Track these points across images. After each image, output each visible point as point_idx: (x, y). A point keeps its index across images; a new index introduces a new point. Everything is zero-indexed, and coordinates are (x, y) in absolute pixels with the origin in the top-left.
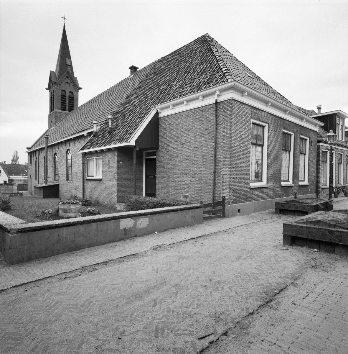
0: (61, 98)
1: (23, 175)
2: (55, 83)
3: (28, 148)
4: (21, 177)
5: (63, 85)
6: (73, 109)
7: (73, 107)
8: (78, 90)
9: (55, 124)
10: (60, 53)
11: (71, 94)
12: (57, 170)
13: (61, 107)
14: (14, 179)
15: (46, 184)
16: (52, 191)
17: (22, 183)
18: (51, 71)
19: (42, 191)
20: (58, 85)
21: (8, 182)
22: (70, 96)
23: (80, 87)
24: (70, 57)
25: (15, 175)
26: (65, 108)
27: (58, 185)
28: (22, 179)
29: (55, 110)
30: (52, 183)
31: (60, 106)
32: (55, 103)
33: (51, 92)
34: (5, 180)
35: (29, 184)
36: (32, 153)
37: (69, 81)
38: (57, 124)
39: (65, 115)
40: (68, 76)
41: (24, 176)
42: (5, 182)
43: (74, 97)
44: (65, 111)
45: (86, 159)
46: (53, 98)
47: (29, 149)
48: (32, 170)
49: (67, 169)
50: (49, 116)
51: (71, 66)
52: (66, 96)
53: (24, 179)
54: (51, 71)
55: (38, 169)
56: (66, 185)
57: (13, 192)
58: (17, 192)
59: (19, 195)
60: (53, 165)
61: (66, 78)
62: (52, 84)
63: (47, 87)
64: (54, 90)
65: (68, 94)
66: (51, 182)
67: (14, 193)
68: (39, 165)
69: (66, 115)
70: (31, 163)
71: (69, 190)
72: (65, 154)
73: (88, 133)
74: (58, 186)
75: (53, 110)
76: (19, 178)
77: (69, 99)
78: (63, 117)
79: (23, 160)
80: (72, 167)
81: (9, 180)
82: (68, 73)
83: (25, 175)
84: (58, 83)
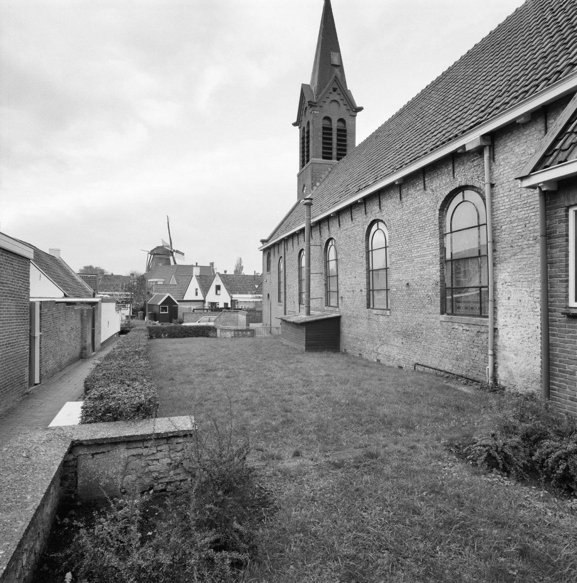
0: (324, 133)
1: (251, 294)
2: (312, 105)
3: (263, 241)
4: (250, 296)
5: (326, 106)
6: (345, 155)
7: (345, 150)
8: (353, 114)
9: (312, 189)
10: (321, 35)
11: (341, 125)
12: (333, 281)
13: (323, 153)
14: (239, 300)
15: (307, 315)
16: (324, 335)
17: (251, 306)
18: (303, 85)
19: (302, 333)
20: (318, 108)
21: (229, 306)
22: (340, 128)
23: (358, 105)
24: (337, 49)
25: (240, 293)
26: (331, 153)
27: (338, 318)
28: (252, 300)
29: (312, 160)
30: (319, 312)
31: (321, 150)
32: (311, 145)
33: (302, 128)
34: (226, 302)
35: (265, 309)
36: (270, 249)
37: (337, 98)
38: (315, 188)
39: (330, 169)
40: (335, 86)
41: (255, 295)
42: (226, 304)
43: (348, 128)
44: (329, 161)
45: (567, 211)
46: (308, 137)
47: (265, 243)
48: (271, 285)
49: (368, 278)
50: (299, 176)
51: (340, 66)
52: (331, 129)
53: (255, 300)
54: (303, 85)
55: (285, 280)
56: (365, 322)
57: (239, 328)
58: (245, 327)
59: (249, 333)
60: (323, 271)
61: (331, 90)
62: (308, 103)
63: (295, 120)
64: (309, 122)
65: (335, 125)
66: (316, 309)
67: (241, 330)
68: (287, 271)
69: (333, 167)
70: (268, 269)
71: (376, 335)
72: (363, 236)
73: (484, 137)
74: (336, 321)
75: (308, 161)
76: (245, 299)
77: (338, 135)
78: (327, 172)
79: (254, 265)
80: (337, 276)
81: (232, 301)
82: (336, 79)
83: (255, 293)
84: (316, 103)
